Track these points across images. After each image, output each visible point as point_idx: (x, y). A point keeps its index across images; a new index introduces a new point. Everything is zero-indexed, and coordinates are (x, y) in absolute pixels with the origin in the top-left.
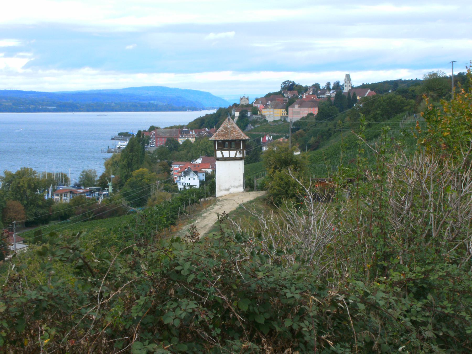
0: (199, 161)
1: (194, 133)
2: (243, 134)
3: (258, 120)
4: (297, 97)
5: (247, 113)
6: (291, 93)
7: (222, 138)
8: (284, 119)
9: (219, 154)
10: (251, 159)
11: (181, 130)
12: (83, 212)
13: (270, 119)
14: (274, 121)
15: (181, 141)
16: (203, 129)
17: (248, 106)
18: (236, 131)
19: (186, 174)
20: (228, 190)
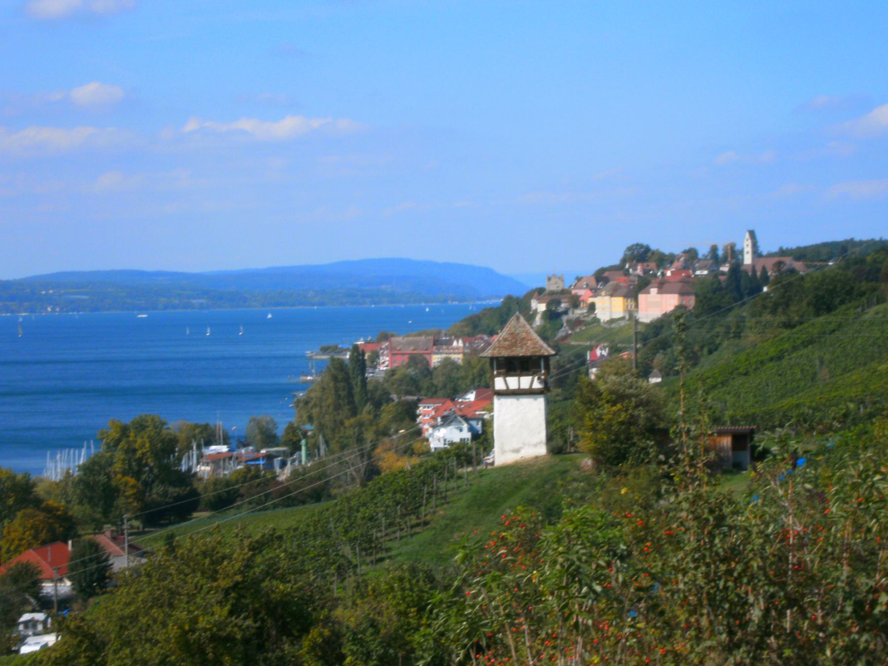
0: (471, 397)
1: (461, 344)
2: (545, 345)
3: (582, 319)
4: (655, 275)
7: (505, 353)
9: (499, 383)
14: (612, 321)
16: (479, 336)
17: (564, 292)
18: (531, 340)
20: (517, 451)
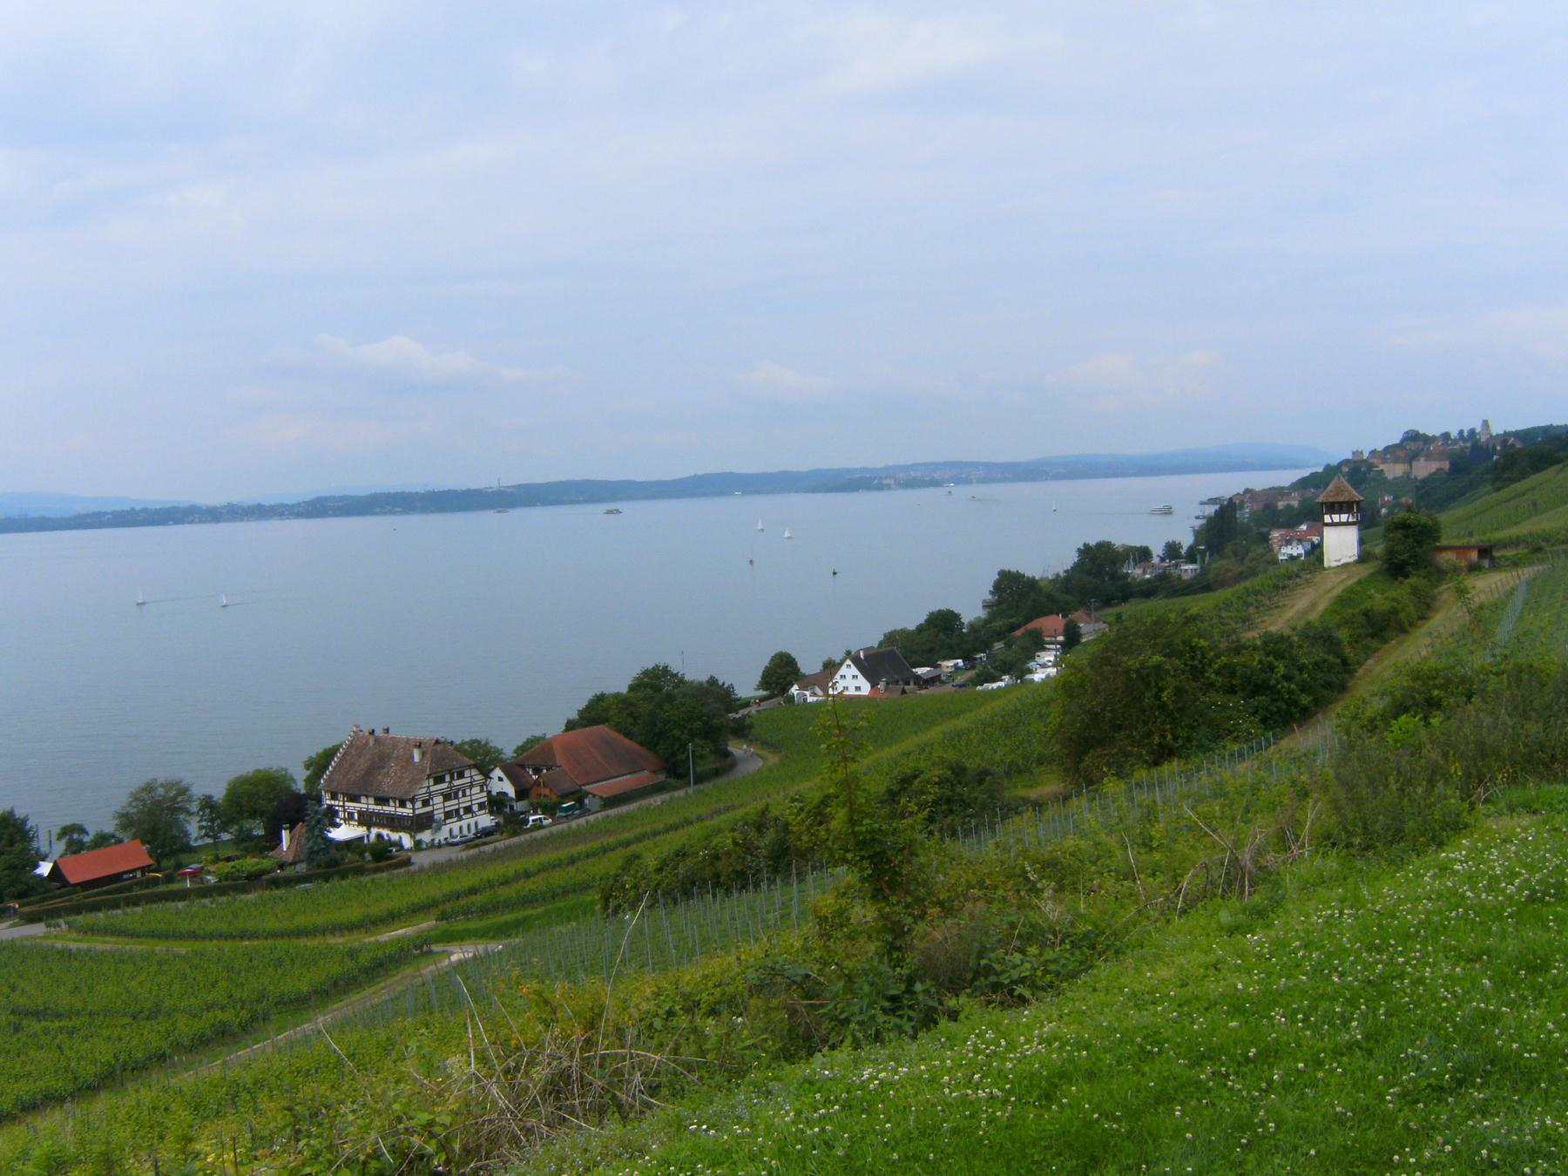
0: (1304, 527)
5: (1358, 470)
6: (1414, 445)
8: (1407, 476)
9: (1327, 519)
10: (1366, 521)
11: (1280, 492)
12: (1163, 586)
13: (1390, 476)
15: (1281, 505)
19: (1288, 543)
